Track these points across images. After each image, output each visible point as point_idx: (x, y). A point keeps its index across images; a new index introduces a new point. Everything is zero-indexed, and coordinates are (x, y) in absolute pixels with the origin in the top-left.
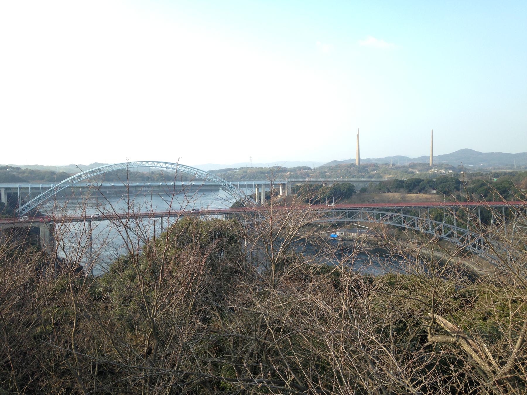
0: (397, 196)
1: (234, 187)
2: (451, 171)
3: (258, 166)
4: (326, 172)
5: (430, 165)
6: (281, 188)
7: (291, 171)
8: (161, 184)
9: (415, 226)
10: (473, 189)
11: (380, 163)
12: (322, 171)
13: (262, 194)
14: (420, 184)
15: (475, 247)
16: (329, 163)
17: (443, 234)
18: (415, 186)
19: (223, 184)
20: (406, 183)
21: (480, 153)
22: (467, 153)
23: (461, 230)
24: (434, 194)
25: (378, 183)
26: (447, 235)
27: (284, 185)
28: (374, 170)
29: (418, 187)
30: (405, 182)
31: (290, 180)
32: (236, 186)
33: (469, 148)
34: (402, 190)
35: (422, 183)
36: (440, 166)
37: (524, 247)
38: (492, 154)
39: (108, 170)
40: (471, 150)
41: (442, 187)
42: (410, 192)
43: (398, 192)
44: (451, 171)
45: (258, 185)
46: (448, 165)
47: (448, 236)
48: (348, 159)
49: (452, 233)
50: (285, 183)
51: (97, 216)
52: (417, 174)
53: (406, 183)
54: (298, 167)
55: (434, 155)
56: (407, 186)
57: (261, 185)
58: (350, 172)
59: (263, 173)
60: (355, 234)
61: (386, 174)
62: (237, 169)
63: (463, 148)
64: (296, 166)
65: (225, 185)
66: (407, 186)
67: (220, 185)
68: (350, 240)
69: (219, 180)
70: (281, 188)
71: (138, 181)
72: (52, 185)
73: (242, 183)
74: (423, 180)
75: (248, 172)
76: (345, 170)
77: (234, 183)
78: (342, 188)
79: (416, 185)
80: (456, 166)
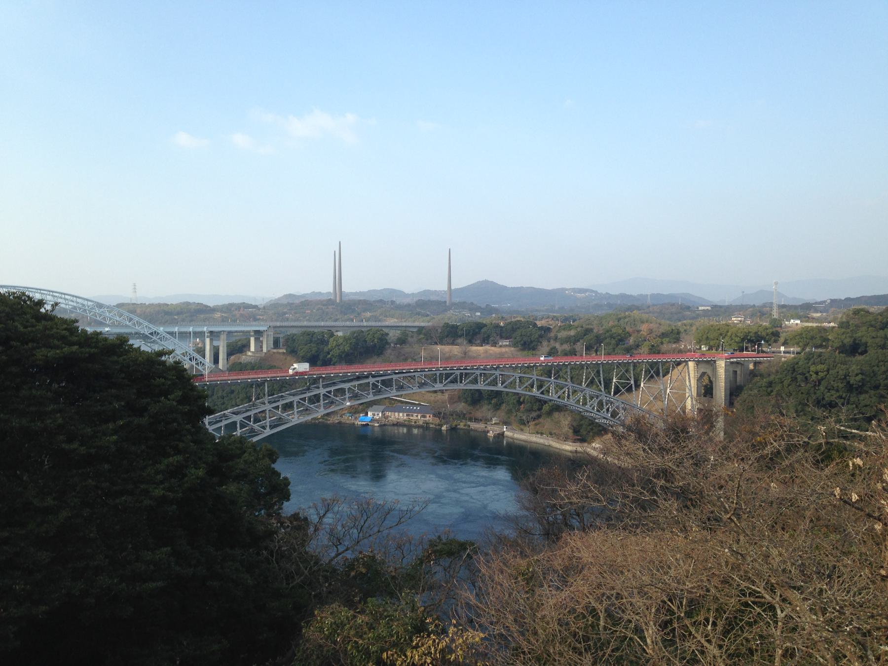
0: (456, 350)
1: (168, 336)
2: (478, 314)
3: (156, 302)
4: (285, 313)
5: (448, 304)
7: (222, 311)
14: (483, 330)
16: (279, 299)
18: (475, 334)
20: (462, 330)
22: (393, 291)
25: (415, 330)
27: (258, 333)
28: (365, 310)
29: (478, 336)
31: (272, 324)
32: (172, 334)
33: (317, 291)
34: (459, 341)
36: (462, 305)
40: (385, 289)
42: (471, 342)
43: (453, 344)
44: (478, 314)
45: (211, 332)
46: (472, 303)
47: (542, 393)
48: (309, 292)
50: (261, 329)
52: (453, 317)
53: (462, 330)
54: (231, 305)
55: (453, 288)
59: (167, 313)
60: (401, 414)
61: (386, 316)
64: (227, 302)
65: (151, 334)
68: (394, 425)
69: (140, 324)
73: (183, 330)
79: (475, 333)
80: (483, 306)
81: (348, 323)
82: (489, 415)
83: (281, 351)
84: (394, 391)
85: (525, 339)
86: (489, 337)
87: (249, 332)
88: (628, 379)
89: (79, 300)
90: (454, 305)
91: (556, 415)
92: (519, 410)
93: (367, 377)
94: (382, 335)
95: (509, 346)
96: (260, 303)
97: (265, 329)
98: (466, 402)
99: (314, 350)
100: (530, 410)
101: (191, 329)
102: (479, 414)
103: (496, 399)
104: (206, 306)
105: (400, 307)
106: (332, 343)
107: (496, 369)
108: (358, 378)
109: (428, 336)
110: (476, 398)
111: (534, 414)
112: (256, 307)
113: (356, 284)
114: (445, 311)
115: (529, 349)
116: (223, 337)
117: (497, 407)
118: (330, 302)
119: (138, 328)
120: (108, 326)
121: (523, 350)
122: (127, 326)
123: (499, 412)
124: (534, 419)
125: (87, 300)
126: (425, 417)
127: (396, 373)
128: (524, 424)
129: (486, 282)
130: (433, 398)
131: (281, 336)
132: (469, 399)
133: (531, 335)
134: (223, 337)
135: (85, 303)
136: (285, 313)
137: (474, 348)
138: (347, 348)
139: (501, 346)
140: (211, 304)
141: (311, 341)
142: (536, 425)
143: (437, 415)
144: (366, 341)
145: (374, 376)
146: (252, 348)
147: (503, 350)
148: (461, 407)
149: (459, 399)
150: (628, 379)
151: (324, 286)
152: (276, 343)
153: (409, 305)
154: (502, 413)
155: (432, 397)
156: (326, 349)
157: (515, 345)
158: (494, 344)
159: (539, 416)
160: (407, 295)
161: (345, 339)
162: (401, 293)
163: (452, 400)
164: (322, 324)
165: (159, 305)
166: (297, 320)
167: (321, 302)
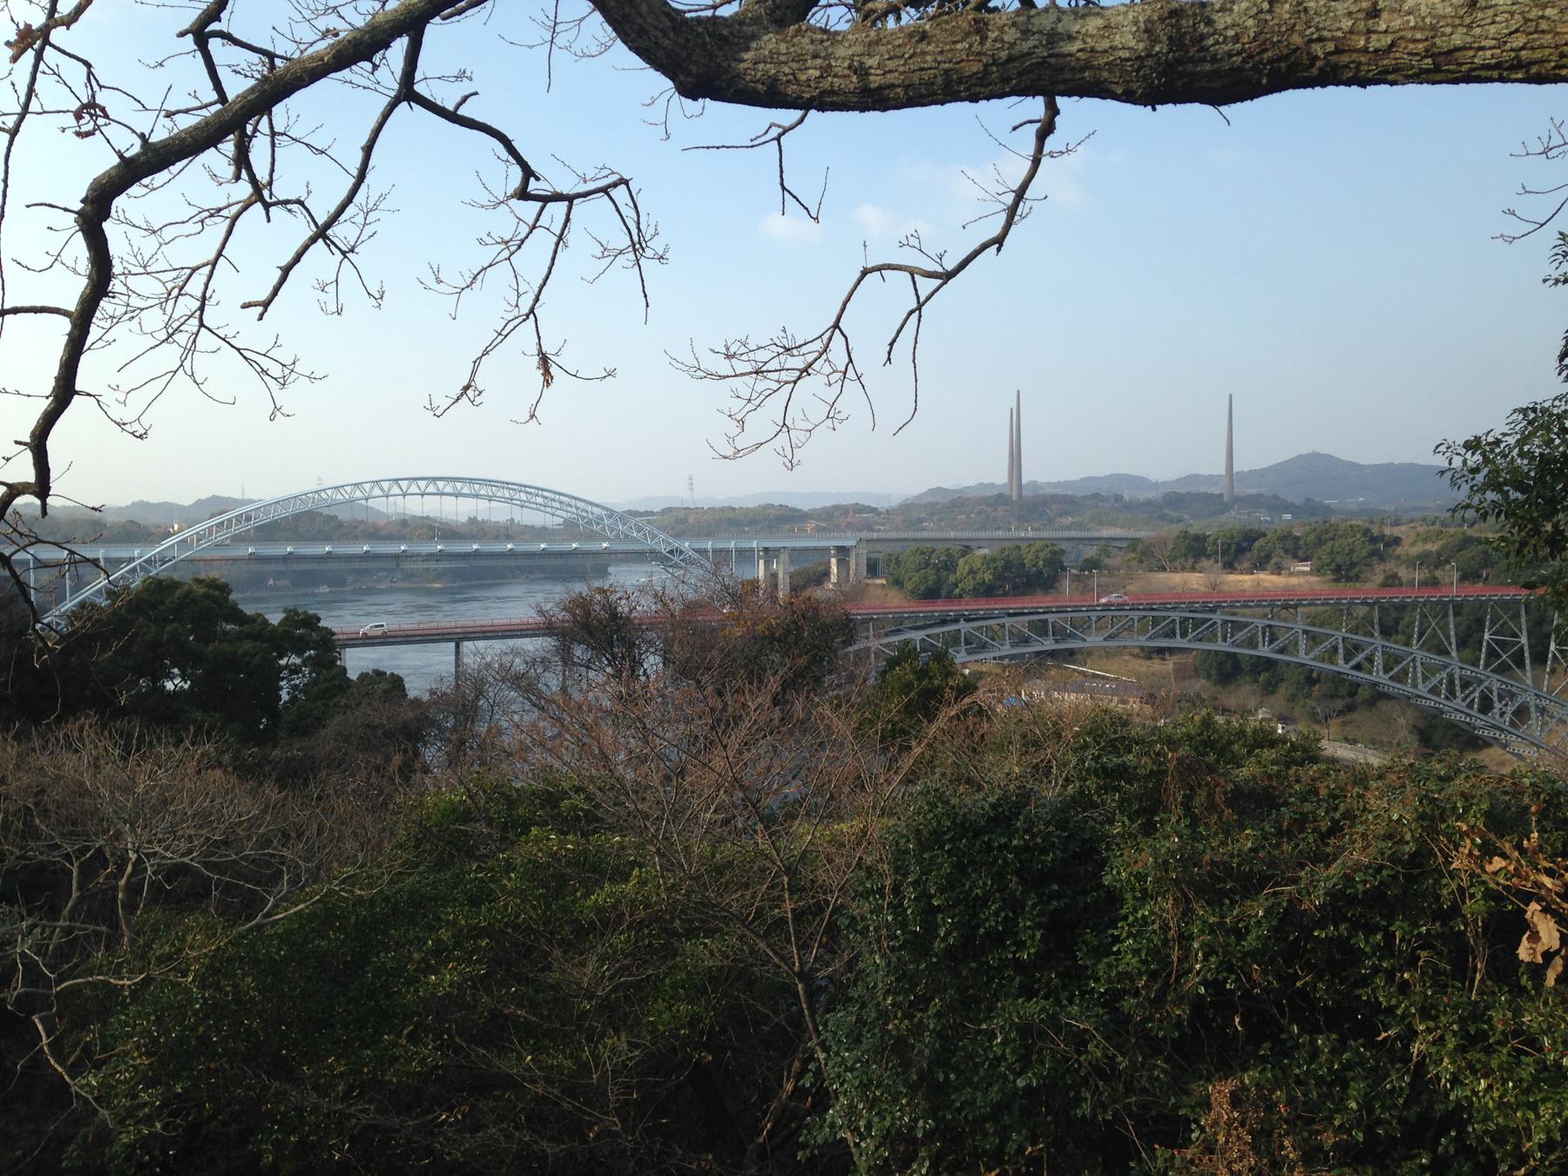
1: (696, 556)
2: (1288, 516)
6: (833, 561)
7: (818, 518)
8: (475, 547)
9: (1255, 647)
10: (1439, 554)
11: (1079, 494)
12: (910, 512)
13: (781, 576)
14: (1257, 544)
15: (1439, 694)
17: (1341, 661)
18: (1241, 550)
19: (663, 548)
20: (1215, 543)
21: (1355, 466)
23: (1397, 647)
24: (1304, 573)
26: (1353, 663)
27: (842, 551)
28: (1063, 513)
29: (1248, 555)
30: (1210, 540)
33: (205, 495)
34: (1205, 563)
35: (1261, 542)
36: (1256, 501)
37: (2, 781)
38: (1389, 466)
39: (272, 516)
40: (1411, 465)
41: (1332, 552)
42: (1230, 567)
43: (1193, 569)
44: (1288, 516)
45: (766, 550)
47: (1358, 667)
48: (973, 484)
49: (1370, 660)
51: (379, 632)
53: (1215, 543)
54: (836, 508)
56: (1216, 553)
57: (777, 550)
58: (995, 519)
62: (651, 513)
63: (1305, 450)
65: (671, 552)
66: (1216, 553)
67: (652, 552)
69: (654, 537)
70: (833, 561)
71: (288, 540)
72: (136, 553)
74: (1264, 535)
75: (691, 520)
76: (979, 514)
77: (697, 546)
78: (1028, 559)
79: (1241, 549)
80: (1299, 501)
81: (1000, 534)
82: (1252, 703)
83: (879, 581)
84: (1007, 646)
85: (1339, 559)
86: (1268, 557)
87: (827, 549)
88: (1516, 636)
89: (580, 504)
90: (1238, 501)
91: (1383, 705)
92: (1309, 695)
93: (956, 621)
94: (1054, 553)
95: (1311, 573)
96: (882, 505)
97: (853, 543)
98: (1209, 676)
99: (932, 579)
100: (1333, 696)
101: (732, 545)
102: (1231, 702)
103: (1267, 673)
104: (794, 510)
105: (1132, 507)
106: (962, 566)
107: (1212, 611)
108: (943, 622)
109: (1146, 555)
110: (1227, 670)
111: (1339, 704)
112: (873, 510)
113: (1049, 467)
114: (1221, 512)
115: (1349, 579)
116: (784, 557)
117: (1270, 688)
118: (1000, 499)
119: (650, 544)
120: (609, 539)
121: (1337, 580)
122: (636, 540)
123: (1272, 699)
124: (1340, 713)
125: (597, 506)
126: (1125, 702)
127: (1010, 615)
128: (1318, 722)
129: (1315, 457)
130: (1144, 669)
131: (880, 556)
132: (1213, 672)
133: (1352, 551)
134: (784, 557)
135: (589, 508)
136: (921, 521)
137: (1232, 577)
138: (988, 577)
139: (1291, 574)
140: (805, 506)
141: (927, 564)
142: (1344, 724)
143: (1150, 699)
144: (1023, 565)
145: (968, 620)
146: (834, 579)
147: (1294, 581)
148: (1200, 685)
149: (1196, 672)
150: (1516, 636)
151: (996, 474)
152: (872, 569)
153: (1148, 503)
154: (1279, 699)
155: (1143, 666)
156: (952, 578)
157: (1317, 571)
158: (1278, 570)
159: (1350, 708)
160: (1157, 485)
161: (988, 562)
162: (1141, 482)
163: (1180, 673)
164: (952, 535)
165: (722, 509)
166: (941, 529)
167: (985, 501)
